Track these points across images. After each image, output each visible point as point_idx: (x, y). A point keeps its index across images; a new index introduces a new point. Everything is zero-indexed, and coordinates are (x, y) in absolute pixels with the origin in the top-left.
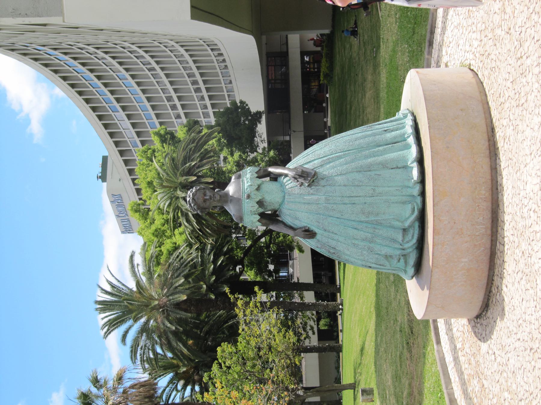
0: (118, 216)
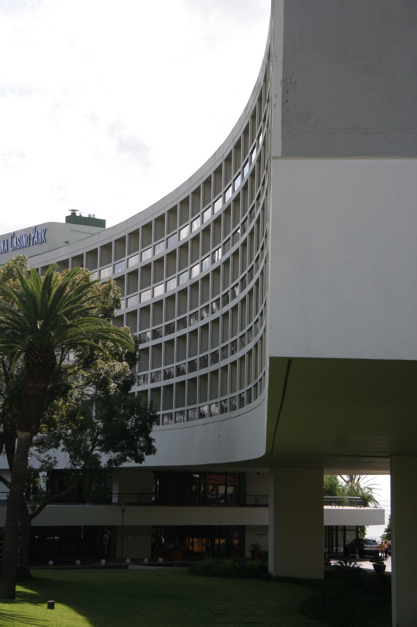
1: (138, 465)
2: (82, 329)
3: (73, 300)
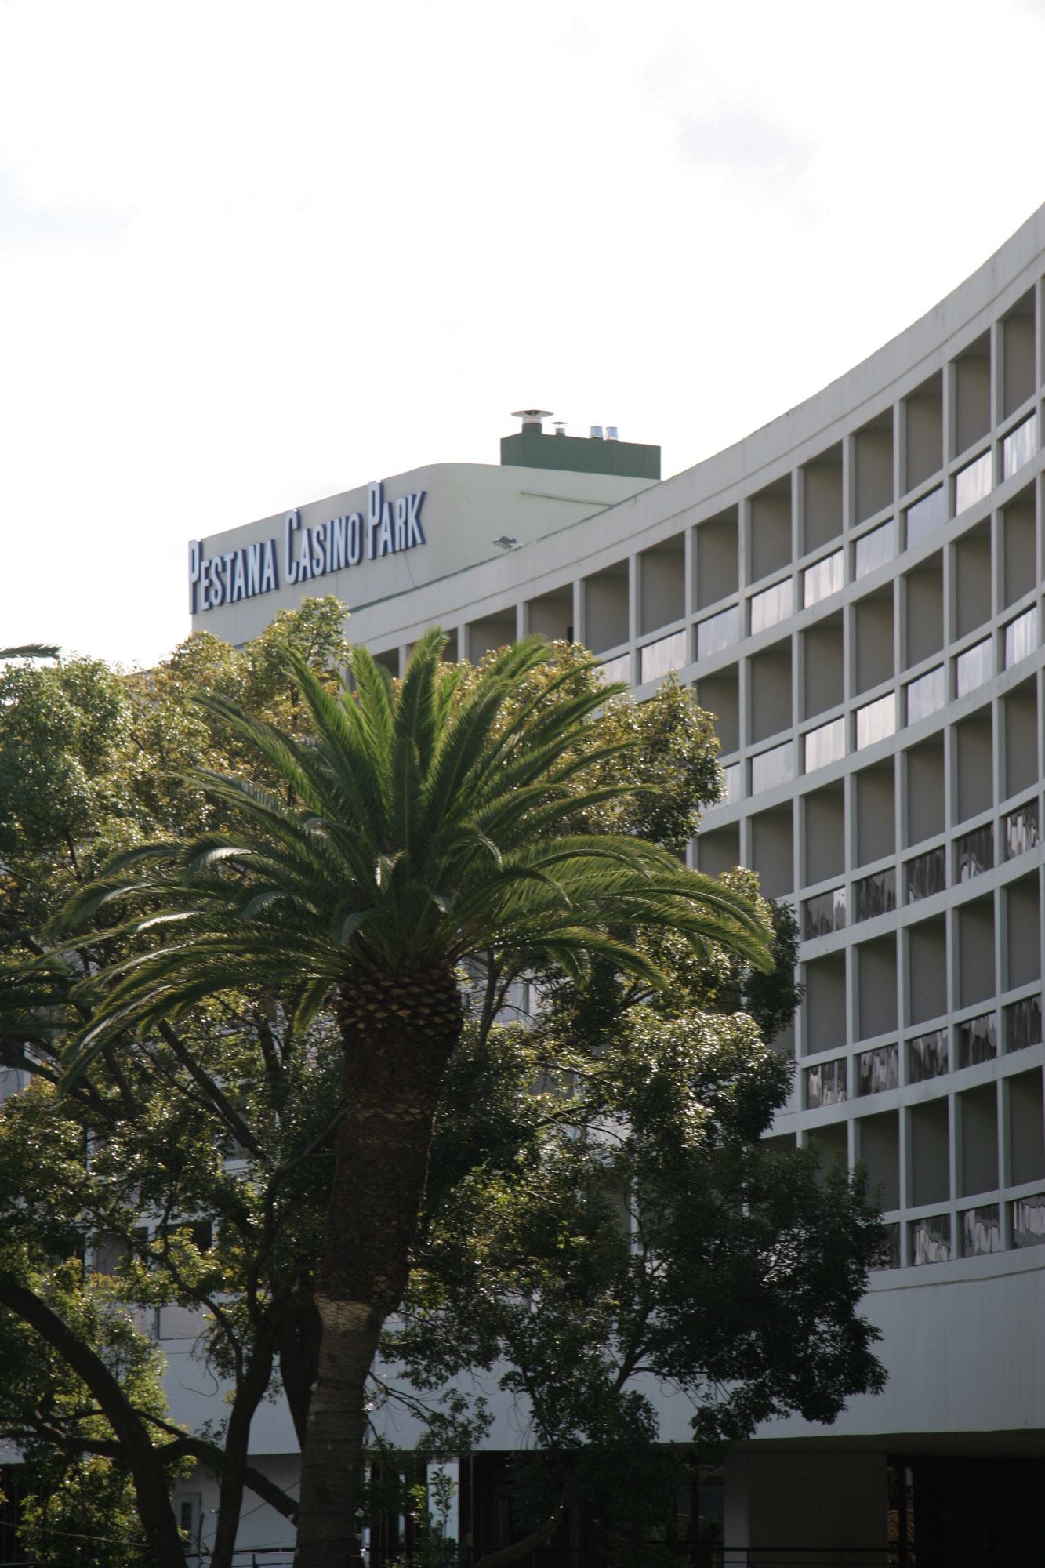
0: (297, 521)
1: (816, 1429)
2: (560, 884)
3: (523, 770)
